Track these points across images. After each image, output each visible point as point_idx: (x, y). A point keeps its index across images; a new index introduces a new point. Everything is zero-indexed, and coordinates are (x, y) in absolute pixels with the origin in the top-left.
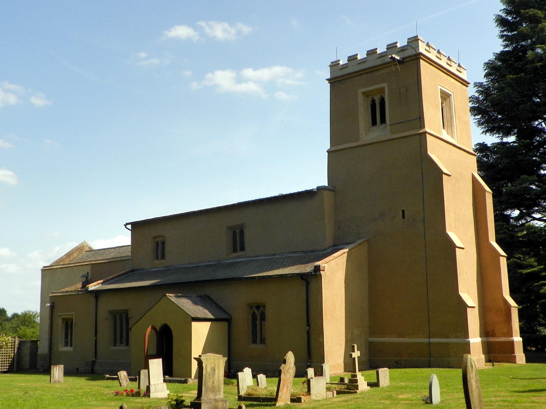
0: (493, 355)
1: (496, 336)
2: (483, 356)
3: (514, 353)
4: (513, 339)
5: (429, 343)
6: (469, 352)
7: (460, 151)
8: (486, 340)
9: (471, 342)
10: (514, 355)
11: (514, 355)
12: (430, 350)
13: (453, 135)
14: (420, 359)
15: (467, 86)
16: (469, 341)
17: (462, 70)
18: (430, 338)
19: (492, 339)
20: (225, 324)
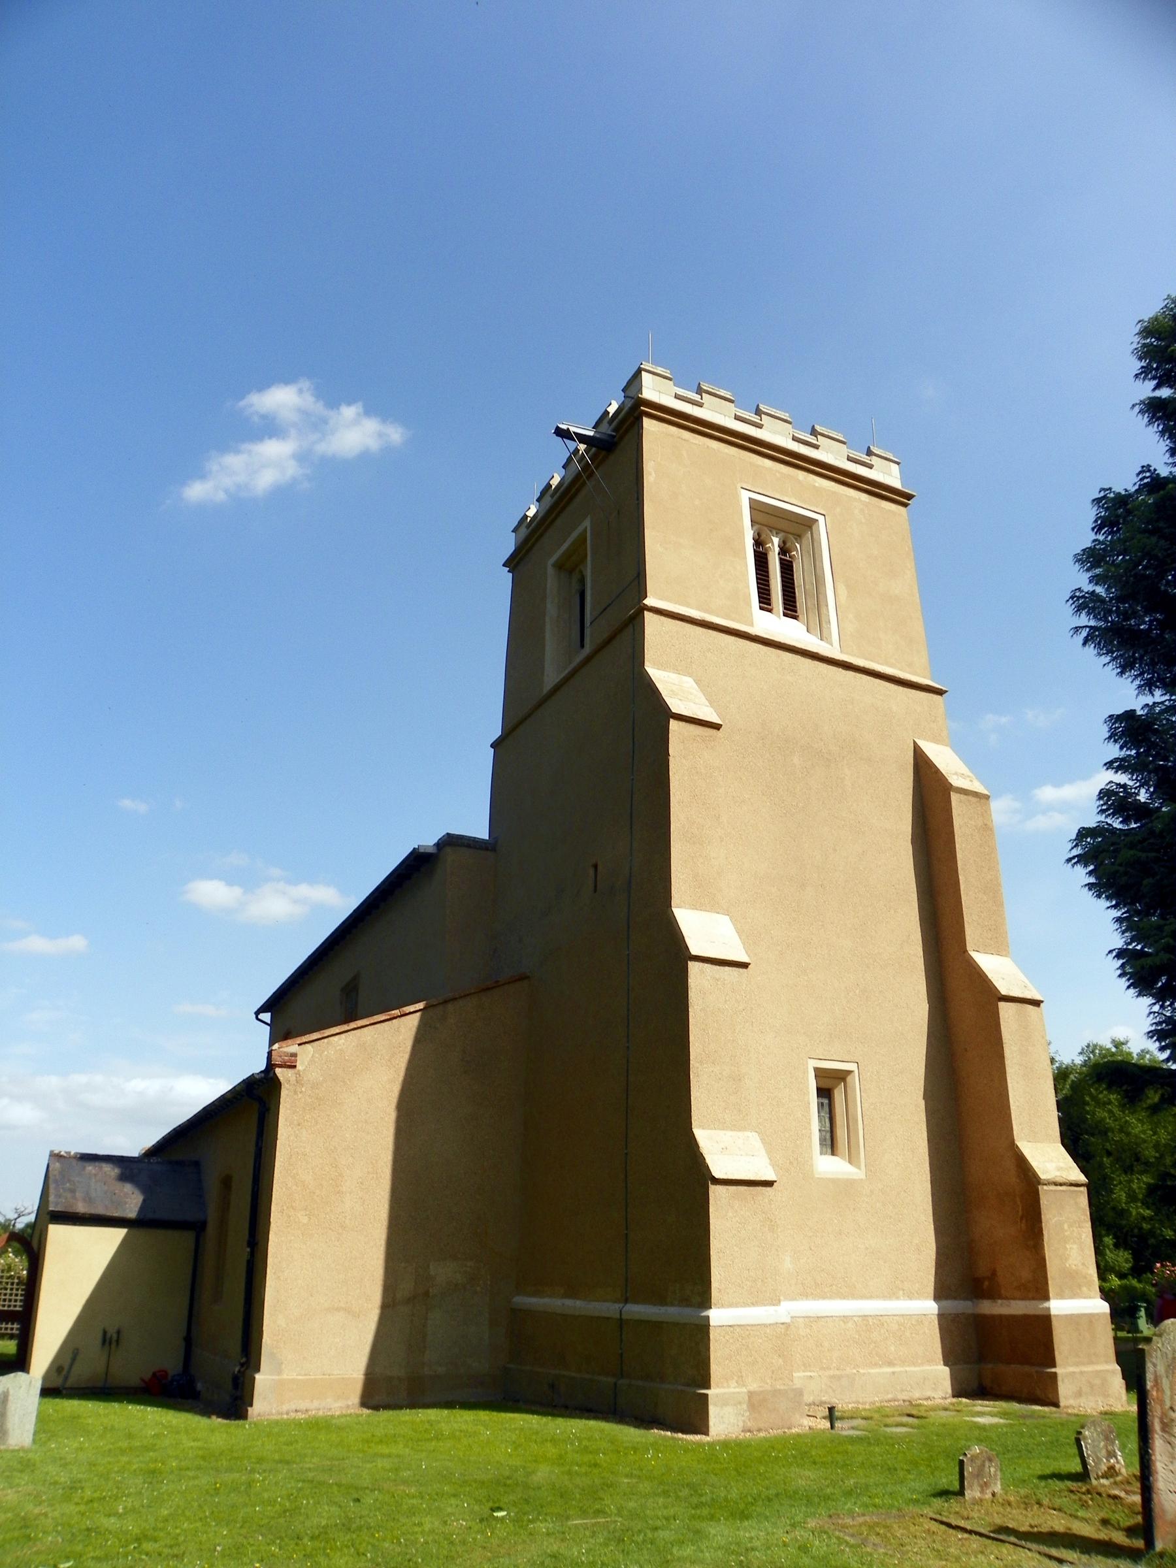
0: (990, 1366)
1: (1000, 1297)
2: (943, 1373)
3: (1054, 1366)
4: (1049, 1309)
5: (621, 1319)
6: (251, 1405)
7: (850, 674)
8: (970, 1311)
9: (712, 1323)
10: (1053, 1370)
11: (1053, 1370)
12: (621, 1349)
13: (824, 630)
14: (1130, 1335)
15: (905, 505)
16: (709, 1317)
17: (874, 460)
18: (626, 1301)
19: (989, 1308)
20: (185, 1240)
